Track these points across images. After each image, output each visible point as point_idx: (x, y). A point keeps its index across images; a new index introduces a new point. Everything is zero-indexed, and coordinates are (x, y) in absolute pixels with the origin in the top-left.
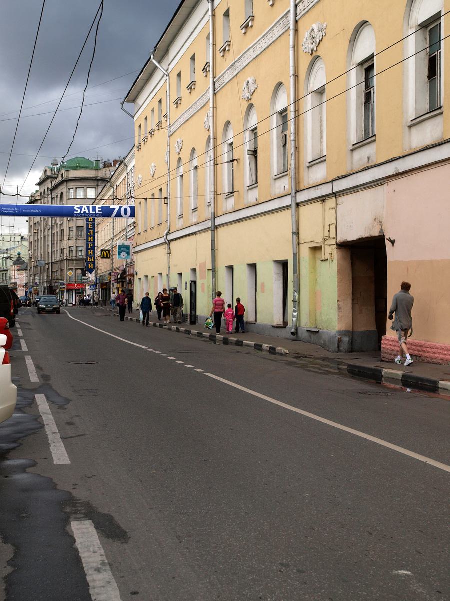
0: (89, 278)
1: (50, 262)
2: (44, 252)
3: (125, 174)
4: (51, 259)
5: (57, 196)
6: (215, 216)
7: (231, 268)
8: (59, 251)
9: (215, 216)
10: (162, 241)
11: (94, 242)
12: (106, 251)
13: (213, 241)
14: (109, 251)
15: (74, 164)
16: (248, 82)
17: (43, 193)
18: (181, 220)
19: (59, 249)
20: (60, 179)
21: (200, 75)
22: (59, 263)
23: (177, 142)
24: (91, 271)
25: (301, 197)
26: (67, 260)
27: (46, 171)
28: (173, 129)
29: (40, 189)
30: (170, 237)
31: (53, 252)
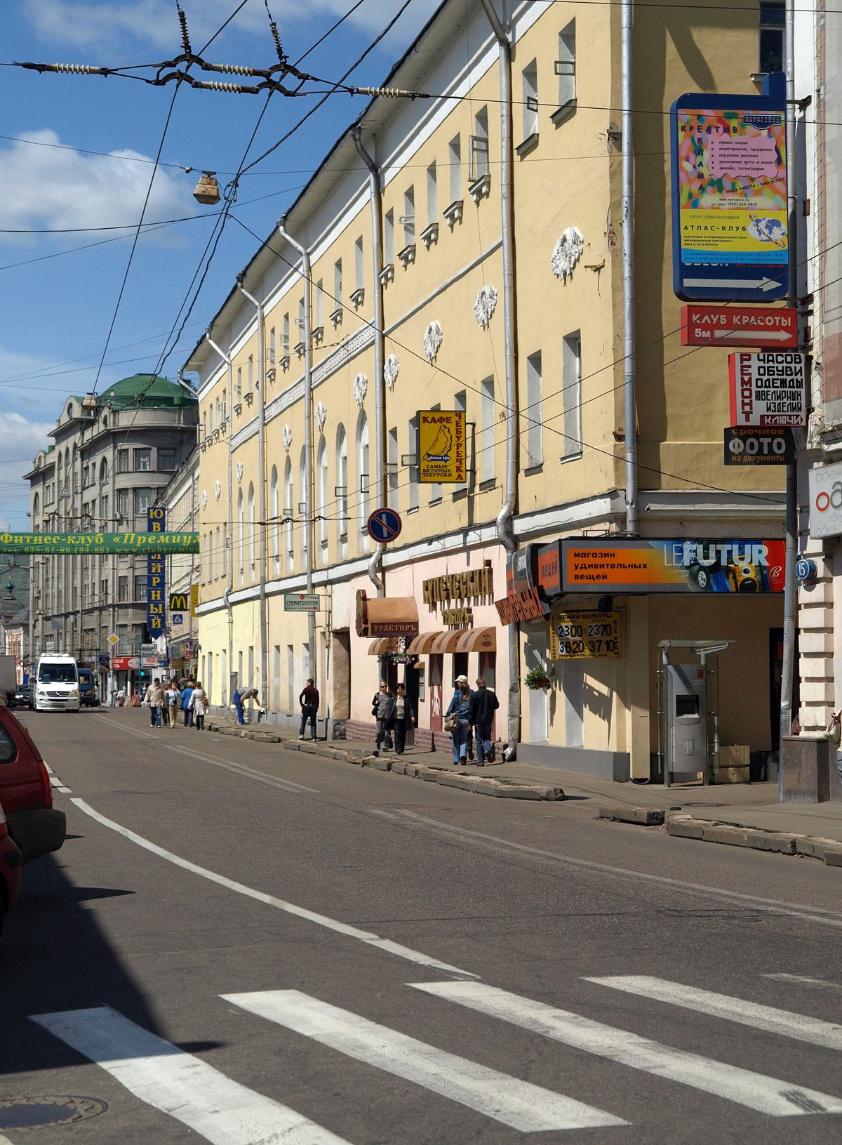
0: (156, 646)
1: (79, 608)
2: (66, 588)
3: (190, 482)
4: (79, 603)
5: (94, 464)
6: (264, 582)
7: (278, 648)
8: (97, 585)
9: (264, 582)
10: (220, 603)
11: (162, 575)
12: (179, 596)
13: (263, 613)
14: (185, 596)
15: (135, 392)
16: (564, 240)
17: (63, 454)
18: (345, 546)
19: (97, 581)
20: (98, 429)
21: (294, 357)
22: (96, 613)
23: (478, 296)
24: (157, 634)
25: (473, 537)
26: (113, 606)
27: (71, 405)
28: (235, 443)
29: (57, 443)
30: (232, 598)
31: (84, 587)
